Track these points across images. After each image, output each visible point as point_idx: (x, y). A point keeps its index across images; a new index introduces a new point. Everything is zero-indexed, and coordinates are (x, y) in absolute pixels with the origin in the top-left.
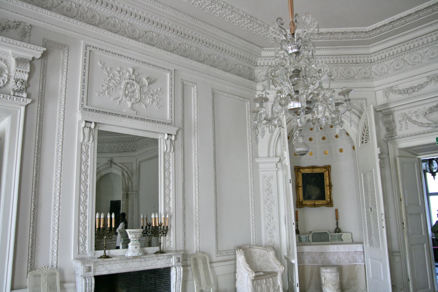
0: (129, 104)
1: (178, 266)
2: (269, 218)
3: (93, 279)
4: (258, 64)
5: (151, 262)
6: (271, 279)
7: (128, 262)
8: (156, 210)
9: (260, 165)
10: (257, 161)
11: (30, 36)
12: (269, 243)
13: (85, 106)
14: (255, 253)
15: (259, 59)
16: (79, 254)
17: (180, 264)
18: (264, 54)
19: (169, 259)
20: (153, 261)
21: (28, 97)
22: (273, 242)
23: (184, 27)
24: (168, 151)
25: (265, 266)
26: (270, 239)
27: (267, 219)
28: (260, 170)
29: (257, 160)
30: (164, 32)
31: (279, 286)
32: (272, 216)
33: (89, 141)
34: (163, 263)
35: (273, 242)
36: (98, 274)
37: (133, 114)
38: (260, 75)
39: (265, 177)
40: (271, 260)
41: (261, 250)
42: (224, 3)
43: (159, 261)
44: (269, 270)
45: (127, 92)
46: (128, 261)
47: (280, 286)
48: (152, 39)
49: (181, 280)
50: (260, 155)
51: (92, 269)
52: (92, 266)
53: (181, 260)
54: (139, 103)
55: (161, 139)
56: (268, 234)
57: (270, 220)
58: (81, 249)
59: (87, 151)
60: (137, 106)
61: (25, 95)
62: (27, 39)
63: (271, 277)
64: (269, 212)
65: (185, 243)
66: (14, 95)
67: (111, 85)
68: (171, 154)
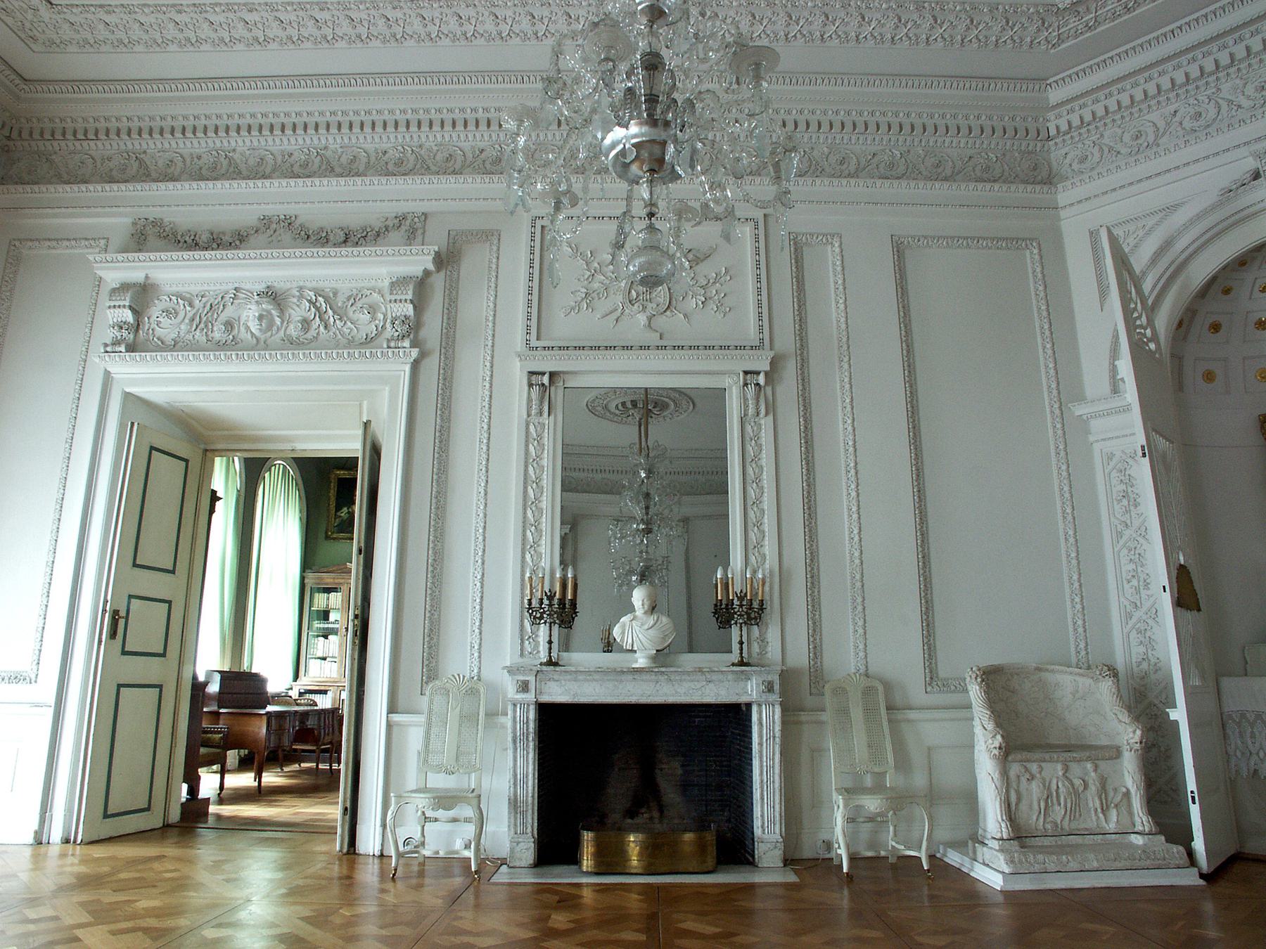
0: (642, 319)
1: (768, 703)
2: (1134, 582)
3: (532, 708)
4: (1053, 132)
5: (686, 685)
6: (1089, 766)
7: (621, 681)
8: (723, 558)
9: (1095, 425)
10: (1077, 413)
11: (424, 233)
12: (1139, 664)
13: (534, 343)
14: (1057, 684)
15: (1051, 115)
16: (522, 655)
17: (775, 697)
18: (1055, 96)
19: (742, 684)
20: (692, 685)
21: (413, 345)
22: (1153, 661)
23: (895, 109)
24: (751, 411)
25: (1092, 729)
26: (1142, 649)
27: (1126, 586)
28: (1091, 438)
29: (1080, 410)
30: (993, 142)
31: (1127, 794)
32: (1142, 577)
33: (541, 414)
34: (723, 692)
35: (1153, 661)
36: (545, 699)
37: (653, 339)
38: (1067, 161)
39: (1111, 457)
40: (1108, 709)
41: (1077, 678)
42: (1036, 5)
43: (711, 685)
44: (1104, 741)
45: (634, 293)
46: (623, 677)
47: (1133, 791)
48: (988, 167)
49: (778, 740)
50: (1089, 392)
51: (532, 686)
52: (531, 679)
53: (777, 687)
54: (668, 313)
55: (730, 388)
56: (1133, 634)
57: (1138, 591)
58: (528, 647)
59: (540, 436)
60: (661, 322)
61: (407, 343)
62: (419, 239)
63: (1089, 759)
64: (1132, 566)
65: (816, 649)
66: (389, 347)
67: (596, 285)
68: (763, 422)
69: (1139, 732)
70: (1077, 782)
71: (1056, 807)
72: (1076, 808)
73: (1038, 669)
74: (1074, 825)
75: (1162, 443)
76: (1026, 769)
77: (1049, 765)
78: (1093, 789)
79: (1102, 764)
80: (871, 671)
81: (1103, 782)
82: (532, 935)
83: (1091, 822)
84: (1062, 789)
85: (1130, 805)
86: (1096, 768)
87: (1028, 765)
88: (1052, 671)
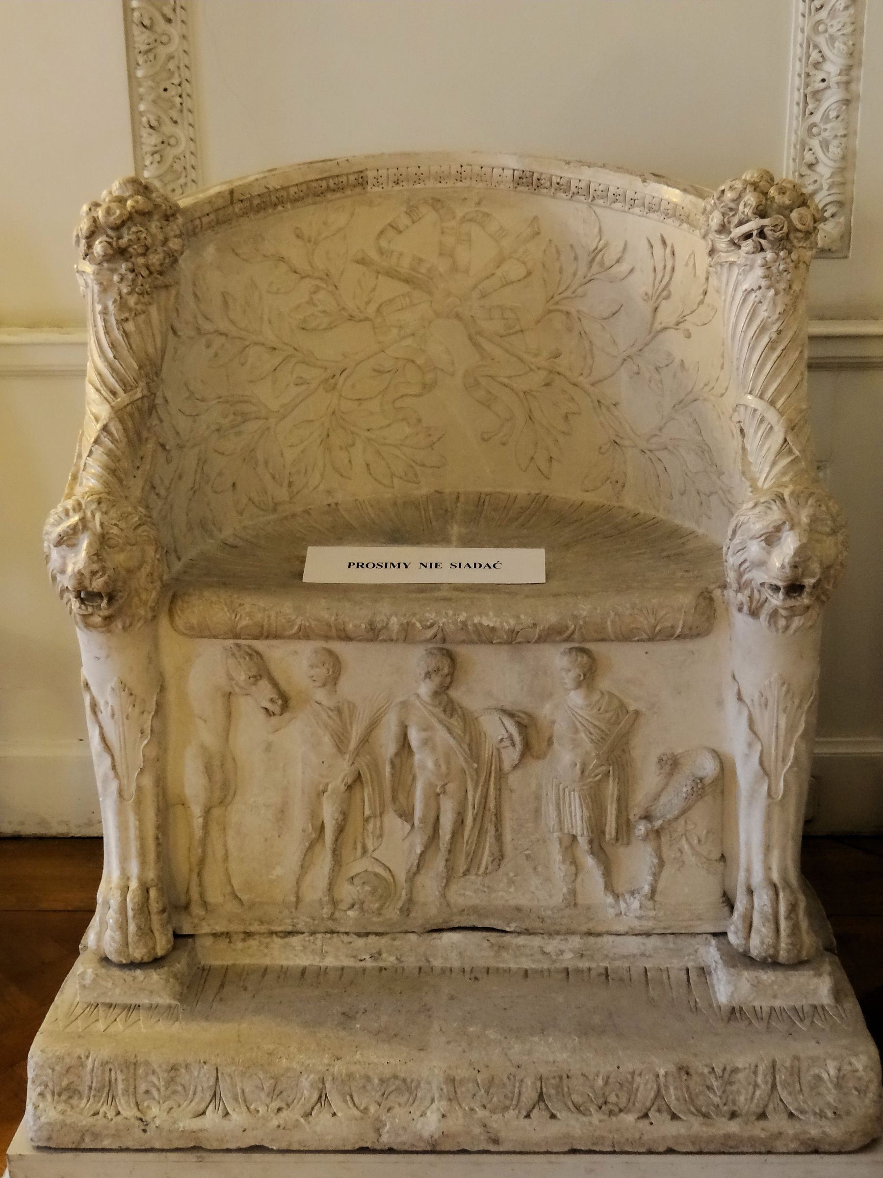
31: (719, 787)
47: (746, 773)
69: (789, 544)
70: (496, 730)
71: (393, 822)
72: (478, 830)
73: (528, 181)
74: (467, 894)
75: (724, 958)
76: (262, 671)
77: (374, 653)
78: (566, 758)
79: (625, 663)
80: (208, 267)
81: (615, 753)
82: (238, 628)
83: (541, 887)
84: (424, 762)
85: (723, 828)
86: (589, 676)
87: (277, 653)
88: (586, 192)
